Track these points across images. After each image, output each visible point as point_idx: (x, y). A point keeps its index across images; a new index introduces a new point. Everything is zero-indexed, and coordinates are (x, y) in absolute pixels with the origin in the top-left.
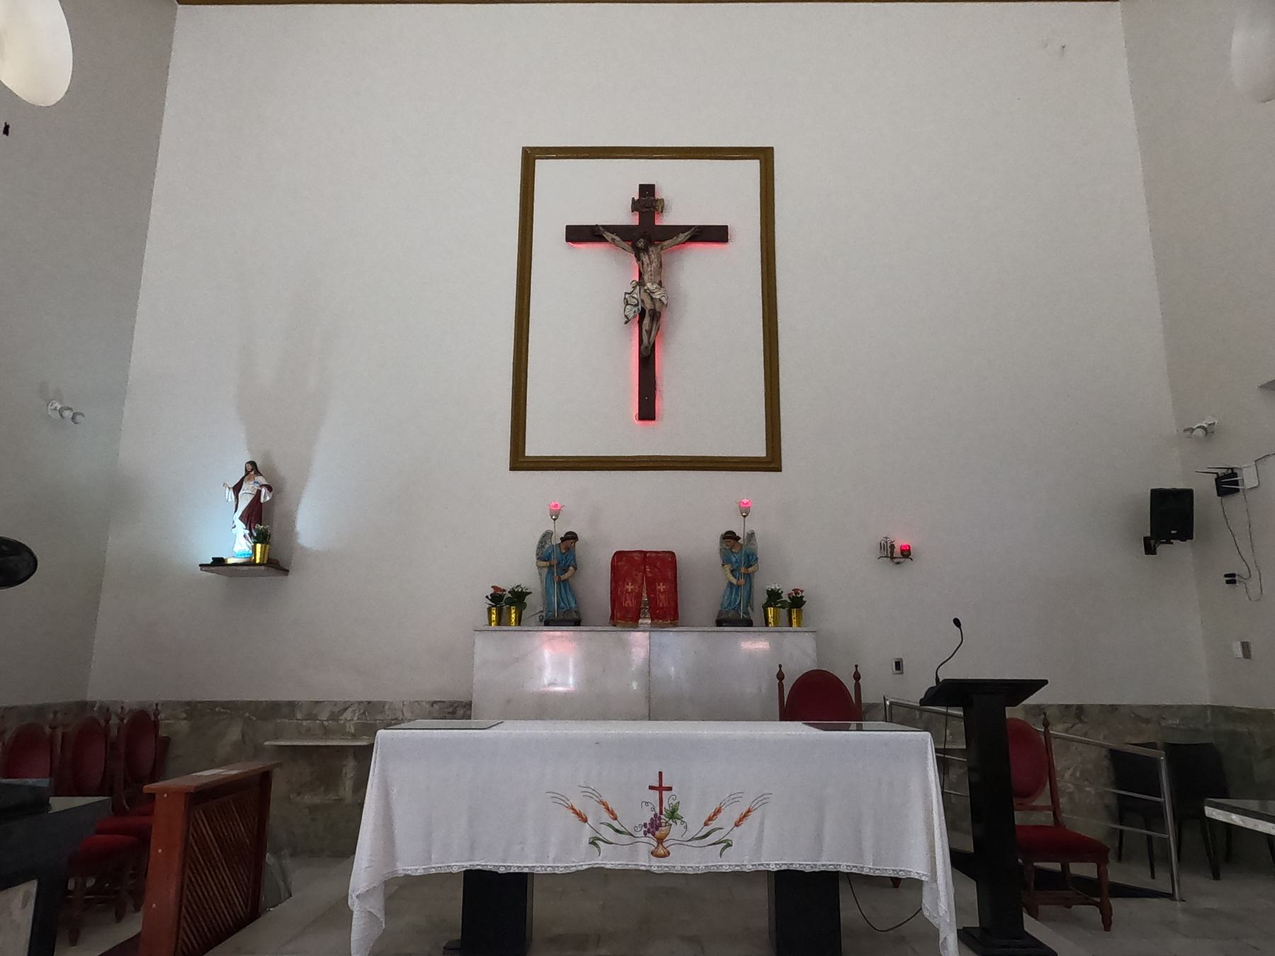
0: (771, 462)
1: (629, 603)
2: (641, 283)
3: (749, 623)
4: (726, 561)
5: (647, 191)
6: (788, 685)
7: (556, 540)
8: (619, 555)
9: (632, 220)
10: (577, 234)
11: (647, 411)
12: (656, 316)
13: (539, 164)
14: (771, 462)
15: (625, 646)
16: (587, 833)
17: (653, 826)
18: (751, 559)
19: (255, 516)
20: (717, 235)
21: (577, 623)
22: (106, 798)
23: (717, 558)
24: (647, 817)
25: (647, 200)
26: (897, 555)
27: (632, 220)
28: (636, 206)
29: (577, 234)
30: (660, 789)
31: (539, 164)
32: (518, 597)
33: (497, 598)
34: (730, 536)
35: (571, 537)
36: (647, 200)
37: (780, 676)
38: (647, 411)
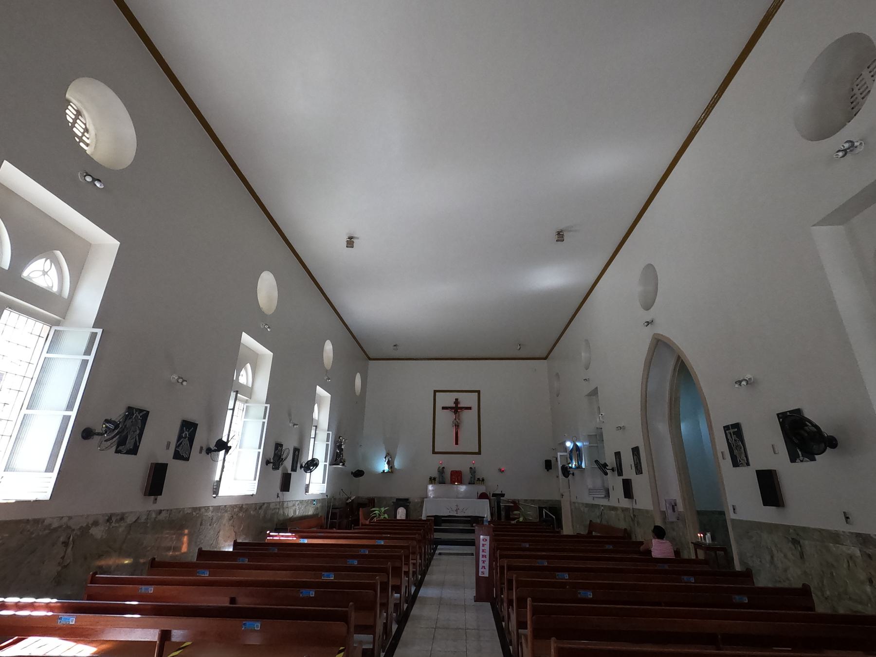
0: (479, 453)
1: (454, 480)
2: (456, 419)
3: (474, 484)
4: (470, 472)
5: (457, 400)
6: (479, 495)
7: (441, 468)
8: (452, 471)
9: (454, 406)
10: (444, 408)
11: (457, 443)
12: (458, 426)
13: (437, 393)
14: (479, 453)
15: (229, 546)
16: (449, 511)
17: (456, 510)
18: (475, 472)
19: (388, 463)
20: (470, 408)
21: (445, 483)
22: (55, 600)
23: (469, 472)
24: (455, 509)
25: (457, 402)
26: (501, 471)
27: (454, 406)
28: (455, 403)
29: (444, 408)
30: (457, 506)
31: (437, 393)
32: (435, 479)
33: (430, 478)
34: (471, 468)
35: (444, 468)
36: (457, 402)
37: (478, 493)
38: (457, 443)
